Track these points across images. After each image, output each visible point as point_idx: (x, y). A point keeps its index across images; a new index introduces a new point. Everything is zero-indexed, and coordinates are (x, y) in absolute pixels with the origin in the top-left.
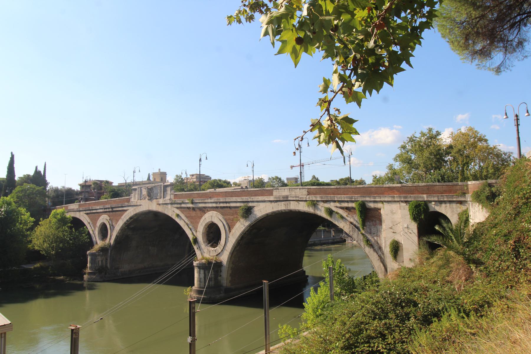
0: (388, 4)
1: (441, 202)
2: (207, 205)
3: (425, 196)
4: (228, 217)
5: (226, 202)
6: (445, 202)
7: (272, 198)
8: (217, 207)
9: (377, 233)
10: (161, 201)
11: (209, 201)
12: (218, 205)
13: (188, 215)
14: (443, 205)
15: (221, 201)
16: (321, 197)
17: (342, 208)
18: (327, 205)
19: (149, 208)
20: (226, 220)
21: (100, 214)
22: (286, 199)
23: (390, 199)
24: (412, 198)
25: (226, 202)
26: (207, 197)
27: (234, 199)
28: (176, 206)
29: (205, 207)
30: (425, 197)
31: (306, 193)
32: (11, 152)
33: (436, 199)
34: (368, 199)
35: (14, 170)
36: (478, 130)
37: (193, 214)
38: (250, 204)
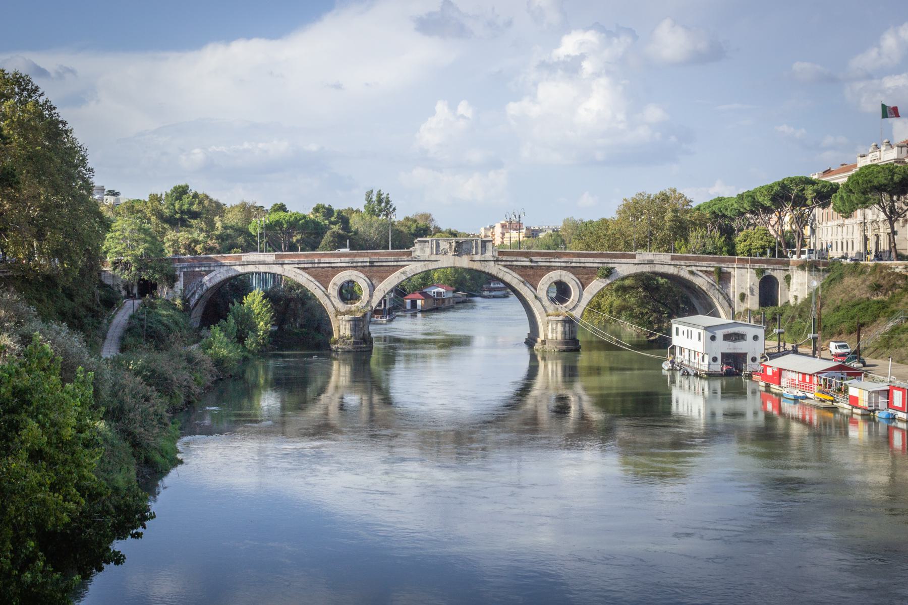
0: (405, 436)
1: (774, 269)
2: (553, 264)
3: (765, 265)
4: (581, 276)
5: (580, 263)
6: (777, 269)
7: (636, 261)
8: (566, 267)
9: (727, 287)
10: (478, 257)
11: (557, 260)
12: (568, 265)
13: (522, 273)
14: (775, 271)
15: (574, 261)
16: (685, 263)
17: (700, 271)
18: (690, 269)
19: (454, 263)
20: (367, 277)
21: (342, 269)
22: (651, 263)
23: (741, 266)
24: (757, 266)
25: (580, 263)
26: (554, 256)
27: (591, 260)
28: (503, 263)
29: (549, 267)
30: (765, 266)
31: (670, 258)
32: (147, 529)
33: (772, 268)
34: (723, 265)
35: (249, 37)
36: (648, 192)
37: (531, 272)
38: (610, 265)
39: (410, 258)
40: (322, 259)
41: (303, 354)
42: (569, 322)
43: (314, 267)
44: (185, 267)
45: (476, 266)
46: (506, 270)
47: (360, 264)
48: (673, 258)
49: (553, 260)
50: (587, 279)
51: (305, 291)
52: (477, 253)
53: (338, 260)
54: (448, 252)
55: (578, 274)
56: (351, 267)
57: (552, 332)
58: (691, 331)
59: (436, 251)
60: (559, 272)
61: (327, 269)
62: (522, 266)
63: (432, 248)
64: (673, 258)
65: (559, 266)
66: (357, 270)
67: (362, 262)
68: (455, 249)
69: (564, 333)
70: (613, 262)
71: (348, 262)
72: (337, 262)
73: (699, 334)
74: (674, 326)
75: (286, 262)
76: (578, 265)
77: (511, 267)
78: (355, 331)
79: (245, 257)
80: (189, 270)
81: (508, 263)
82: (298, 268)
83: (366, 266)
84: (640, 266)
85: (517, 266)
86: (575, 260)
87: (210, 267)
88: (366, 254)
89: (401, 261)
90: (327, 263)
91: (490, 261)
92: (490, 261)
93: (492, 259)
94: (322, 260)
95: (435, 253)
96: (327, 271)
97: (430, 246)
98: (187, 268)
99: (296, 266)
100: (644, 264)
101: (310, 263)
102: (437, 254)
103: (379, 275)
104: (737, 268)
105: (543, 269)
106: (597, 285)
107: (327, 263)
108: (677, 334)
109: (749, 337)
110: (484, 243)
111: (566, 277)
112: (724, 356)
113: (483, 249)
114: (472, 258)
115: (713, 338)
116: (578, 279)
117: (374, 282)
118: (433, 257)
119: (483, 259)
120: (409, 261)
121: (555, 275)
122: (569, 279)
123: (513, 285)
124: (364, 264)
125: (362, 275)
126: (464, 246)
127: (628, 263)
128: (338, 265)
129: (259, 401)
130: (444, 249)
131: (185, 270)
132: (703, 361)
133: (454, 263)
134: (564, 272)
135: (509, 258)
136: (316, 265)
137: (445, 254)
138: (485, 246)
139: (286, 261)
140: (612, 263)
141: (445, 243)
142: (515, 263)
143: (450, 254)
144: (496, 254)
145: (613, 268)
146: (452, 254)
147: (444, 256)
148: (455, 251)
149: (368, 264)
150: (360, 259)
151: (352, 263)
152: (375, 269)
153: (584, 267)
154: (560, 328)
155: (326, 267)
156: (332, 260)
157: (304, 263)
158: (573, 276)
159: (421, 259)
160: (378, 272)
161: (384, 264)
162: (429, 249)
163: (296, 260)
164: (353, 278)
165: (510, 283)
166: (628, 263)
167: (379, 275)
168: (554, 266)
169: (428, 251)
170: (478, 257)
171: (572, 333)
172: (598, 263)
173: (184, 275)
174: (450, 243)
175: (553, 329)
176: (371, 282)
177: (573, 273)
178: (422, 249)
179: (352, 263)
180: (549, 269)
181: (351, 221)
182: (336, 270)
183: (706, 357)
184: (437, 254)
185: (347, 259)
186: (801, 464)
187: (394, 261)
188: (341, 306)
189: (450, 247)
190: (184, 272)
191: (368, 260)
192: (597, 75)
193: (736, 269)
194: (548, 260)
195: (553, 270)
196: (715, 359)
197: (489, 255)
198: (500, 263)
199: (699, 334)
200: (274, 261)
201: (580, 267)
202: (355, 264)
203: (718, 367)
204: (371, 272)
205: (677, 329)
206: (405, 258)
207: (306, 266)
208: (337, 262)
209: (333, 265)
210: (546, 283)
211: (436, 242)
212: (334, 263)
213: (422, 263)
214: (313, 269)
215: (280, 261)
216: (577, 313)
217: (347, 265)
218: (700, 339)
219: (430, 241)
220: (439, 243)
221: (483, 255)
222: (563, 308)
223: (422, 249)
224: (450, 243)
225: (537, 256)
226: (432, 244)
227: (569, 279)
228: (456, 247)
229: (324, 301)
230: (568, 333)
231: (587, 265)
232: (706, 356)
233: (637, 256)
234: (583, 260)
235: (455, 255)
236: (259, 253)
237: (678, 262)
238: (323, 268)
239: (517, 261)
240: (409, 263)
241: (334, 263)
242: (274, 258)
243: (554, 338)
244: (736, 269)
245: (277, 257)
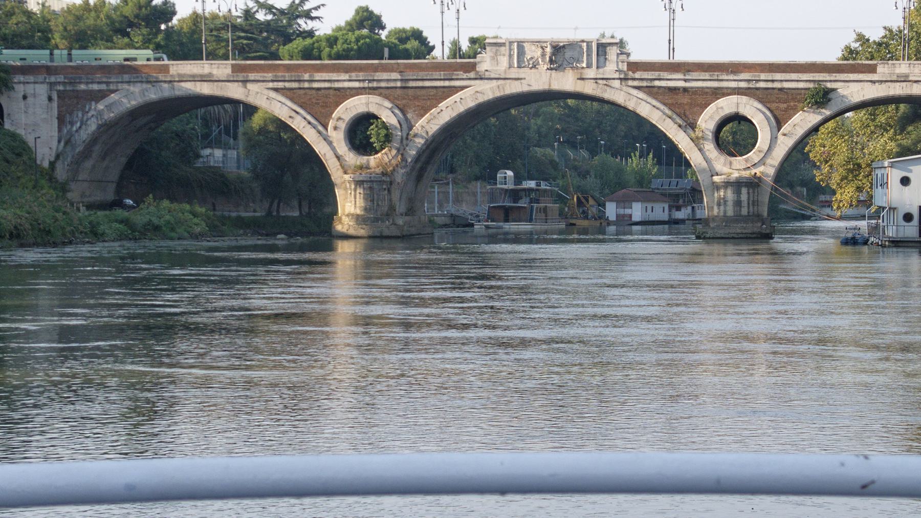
4: (773, 106)
5: (773, 81)
10: (591, 73)
11: (731, 77)
21: (354, 91)
25: (773, 81)
27: (794, 76)
28: (636, 83)
37: (685, 100)
38: (829, 85)
39: (472, 75)
40: (316, 74)
41: (64, 347)
43: (304, 88)
44: (59, 83)
45: (588, 88)
46: (641, 95)
47: (383, 84)
49: (725, 77)
50: (786, 110)
51: (283, 126)
52: (589, 66)
54: (538, 63)
56: (370, 88)
59: (518, 62)
60: (734, 98)
61: (327, 92)
63: (511, 56)
65: (735, 88)
66: (380, 95)
67: (388, 80)
70: (832, 78)
71: (364, 81)
72: (343, 80)
75: (252, 78)
76: (770, 85)
77: (651, 91)
78: (372, 201)
79: (175, 68)
80: (68, 88)
81: (645, 84)
82: (276, 90)
83: (396, 88)
84: (884, 85)
85: (659, 87)
86: (763, 76)
87: (108, 83)
88: (396, 66)
89: (457, 79)
90: (325, 81)
91: (614, 79)
92: (614, 79)
93: (617, 75)
94: (318, 76)
95: (516, 66)
96: (327, 96)
97: (507, 53)
98: (64, 83)
99: (271, 85)
100: (891, 81)
101: (295, 81)
102: (519, 67)
103: (417, 103)
107: (325, 81)
110: (602, 48)
111: (748, 107)
113: (602, 59)
114: (581, 74)
116: (769, 109)
117: (409, 116)
118: (514, 73)
119: (601, 76)
120: (470, 79)
121: (726, 106)
122: (751, 109)
124: (392, 84)
125: (388, 104)
126: (568, 54)
127: (861, 81)
129: (334, 227)
130: (532, 58)
131: (61, 88)
133: (550, 86)
134: (744, 99)
135: (646, 75)
136: (306, 85)
137: (534, 67)
138: (605, 53)
139: (252, 76)
140: (831, 81)
141: (533, 48)
142: (657, 83)
143: (543, 67)
144: (624, 67)
145: (833, 90)
146: (546, 67)
147: (533, 70)
148: (551, 61)
149: (399, 84)
150: (385, 76)
151: (370, 81)
152: (410, 92)
153: (781, 89)
155: (325, 88)
156: (334, 76)
157: (284, 81)
158: (760, 106)
159: (493, 76)
160: (416, 98)
161: (427, 84)
163: (269, 76)
164: (373, 109)
165: (648, 118)
166: (861, 81)
167: (417, 103)
169: (504, 61)
170: (591, 73)
172: (807, 81)
173: (59, 97)
174: (542, 47)
176: (404, 115)
178: (494, 58)
179: (370, 81)
180: (718, 93)
181: (453, 213)
182: (343, 95)
184: (519, 67)
185: (361, 75)
187: (444, 80)
188: (352, 158)
189: (543, 55)
190: (59, 92)
191: (399, 77)
194: (716, 78)
195: (724, 95)
197: (610, 69)
198: (630, 83)
200: (228, 75)
201: (773, 89)
202: (375, 84)
204: (404, 99)
207: (287, 85)
208: (343, 80)
209: (337, 85)
210: (711, 118)
211: (518, 46)
212: (338, 81)
213: (494, 83)
214: (302, 92)
215: (241, 76)
217: (360, 85)
220: (523, 47)
221: (601, 70)
223: (494, 58)
225: (696, 71)
226: (510, 50)
227: (751, 109)
228: (553, 54)
229: (320, 148)
230: (745, 204)
231: (786, 85)
233: (880, 69)
234: (778, 76)
235: (551, 69)
236: (204, 62)
238: (319, 89)
239: (660, 79)
240: (472, 82)
241: (338, 81)
242: (228, 71)
243: (722, 214)
245: (236, 69)
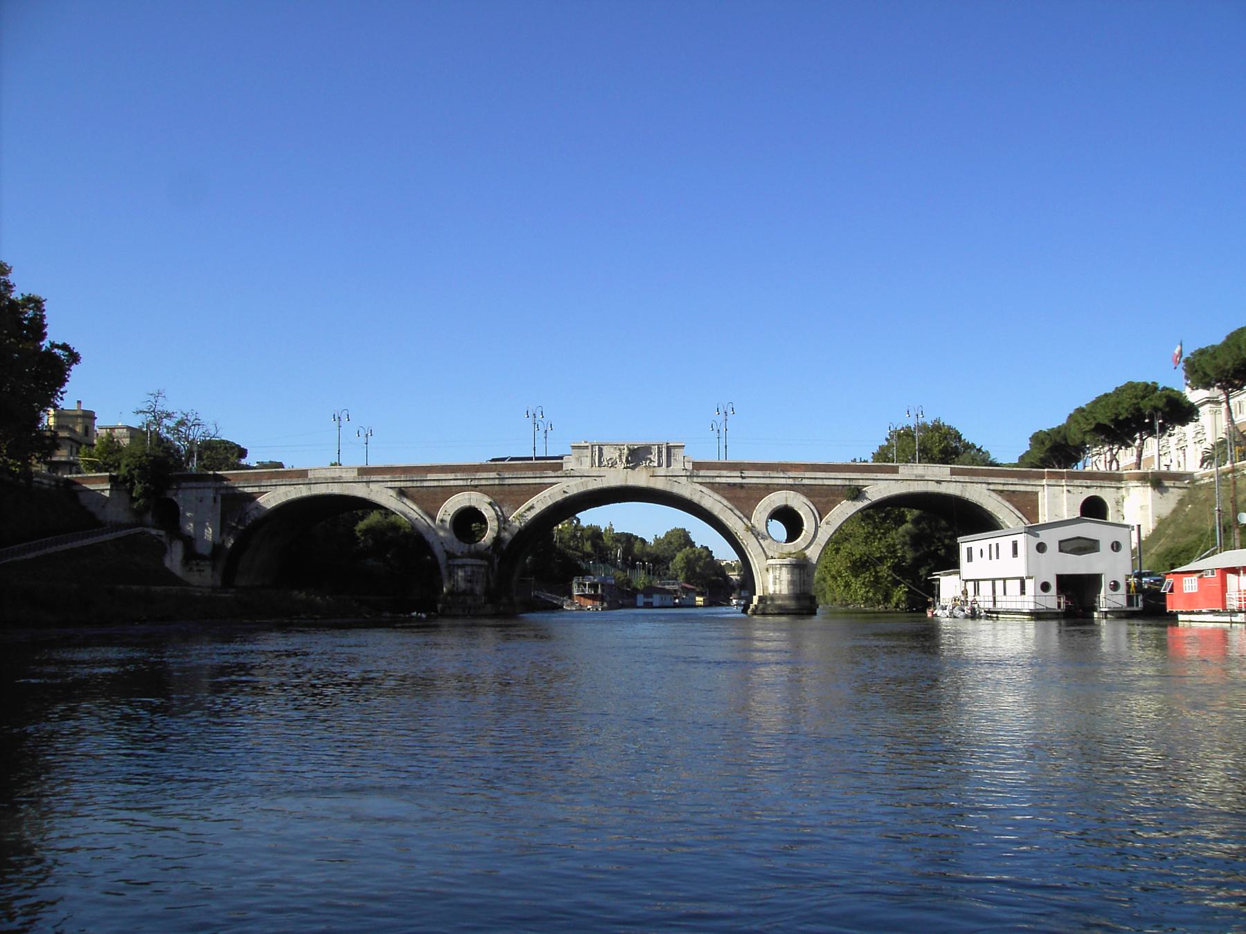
4: (817, 499)
28: (700, 480)
37: (742, 494)
38: (861, 483)
39: (559, 473)
42: (801, 566)
46: (704, 489)
48: (953, 472)
50: (828, 502)
52: (660, 465)
53: (451, 476)
55: (813, 496)
57: (775, 583)
58: (997, 544)
62: (729, 484)
64: (953, 472)
68: (627, 458)
69: (792, 583)
73: (1015, 545)
74: (963, 549)
77: (713, 487)
81: (708, 480)
93: (684, 473)
103: (512, 498)
104: (1048, 485)
105: (760, 489)
106: (845, 510)
108: (970, 559)
109: (1105, 546)
111: (795, 501)
112: (1061, 579)
115: (1041, 548)
123: (716, 513)
128: (452, 483)
132: (1023, 592)
139: (374, 478)
143: (620, 466)
146: (623, 467)
147: (612, 469)
148: (628, 461)
154: (785, 575)
158: (805, 500)
162: (589, 459)
167: (512, 498)
168: (778, 484)
170: (662, 471)
171: (804, 584)
174: (620, 449)
175: (775, 578)
177: (806, 495)
178: (579, 459)
183: (1029, 584)
184: (599, 466)
186: (436, 759)
192: (867, 499)
193: (1046, 487)
195: (775, 490)
196: (1045, 587)
197: (677, 467)
198: (695, 479)
199: (1015, 545)
203: (1051, 601)
205: (970, 550)
206: (551, 473)
216: (813, 554)
218: (1015, 553)
219: (590, 447)
222: (791, 547)
224: (620, 449)
228: (629, 455)
232: (1027, 582)
237: (961, 478)
240: (559, 480)
244: (1046, 487)
